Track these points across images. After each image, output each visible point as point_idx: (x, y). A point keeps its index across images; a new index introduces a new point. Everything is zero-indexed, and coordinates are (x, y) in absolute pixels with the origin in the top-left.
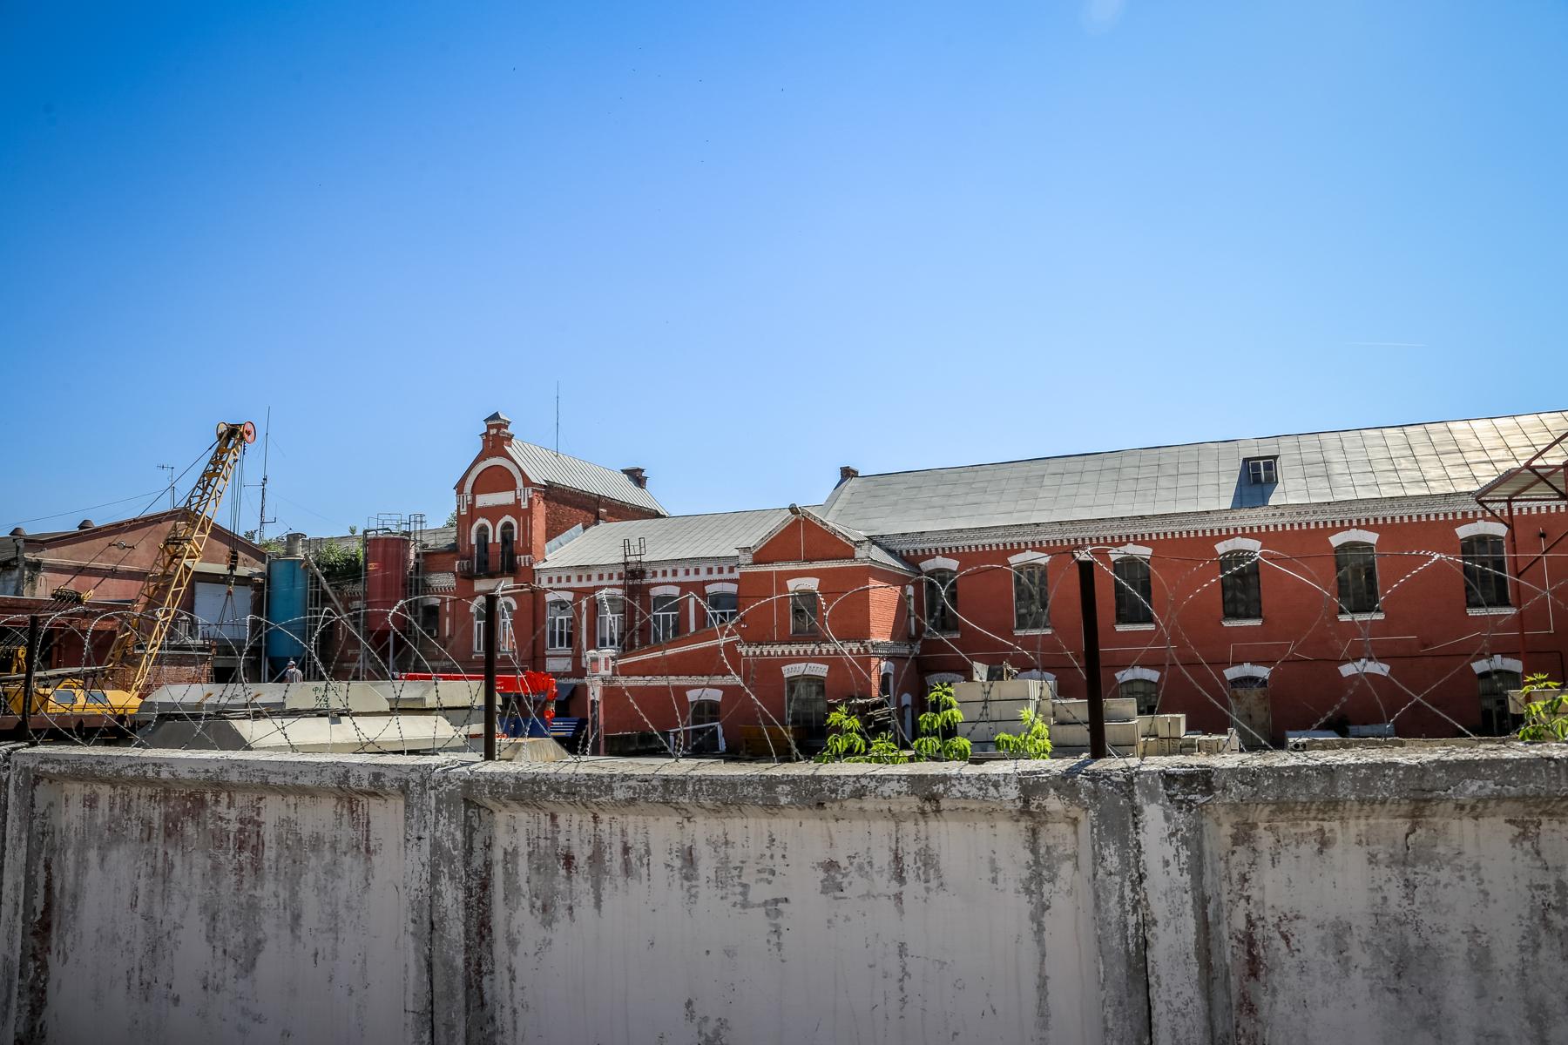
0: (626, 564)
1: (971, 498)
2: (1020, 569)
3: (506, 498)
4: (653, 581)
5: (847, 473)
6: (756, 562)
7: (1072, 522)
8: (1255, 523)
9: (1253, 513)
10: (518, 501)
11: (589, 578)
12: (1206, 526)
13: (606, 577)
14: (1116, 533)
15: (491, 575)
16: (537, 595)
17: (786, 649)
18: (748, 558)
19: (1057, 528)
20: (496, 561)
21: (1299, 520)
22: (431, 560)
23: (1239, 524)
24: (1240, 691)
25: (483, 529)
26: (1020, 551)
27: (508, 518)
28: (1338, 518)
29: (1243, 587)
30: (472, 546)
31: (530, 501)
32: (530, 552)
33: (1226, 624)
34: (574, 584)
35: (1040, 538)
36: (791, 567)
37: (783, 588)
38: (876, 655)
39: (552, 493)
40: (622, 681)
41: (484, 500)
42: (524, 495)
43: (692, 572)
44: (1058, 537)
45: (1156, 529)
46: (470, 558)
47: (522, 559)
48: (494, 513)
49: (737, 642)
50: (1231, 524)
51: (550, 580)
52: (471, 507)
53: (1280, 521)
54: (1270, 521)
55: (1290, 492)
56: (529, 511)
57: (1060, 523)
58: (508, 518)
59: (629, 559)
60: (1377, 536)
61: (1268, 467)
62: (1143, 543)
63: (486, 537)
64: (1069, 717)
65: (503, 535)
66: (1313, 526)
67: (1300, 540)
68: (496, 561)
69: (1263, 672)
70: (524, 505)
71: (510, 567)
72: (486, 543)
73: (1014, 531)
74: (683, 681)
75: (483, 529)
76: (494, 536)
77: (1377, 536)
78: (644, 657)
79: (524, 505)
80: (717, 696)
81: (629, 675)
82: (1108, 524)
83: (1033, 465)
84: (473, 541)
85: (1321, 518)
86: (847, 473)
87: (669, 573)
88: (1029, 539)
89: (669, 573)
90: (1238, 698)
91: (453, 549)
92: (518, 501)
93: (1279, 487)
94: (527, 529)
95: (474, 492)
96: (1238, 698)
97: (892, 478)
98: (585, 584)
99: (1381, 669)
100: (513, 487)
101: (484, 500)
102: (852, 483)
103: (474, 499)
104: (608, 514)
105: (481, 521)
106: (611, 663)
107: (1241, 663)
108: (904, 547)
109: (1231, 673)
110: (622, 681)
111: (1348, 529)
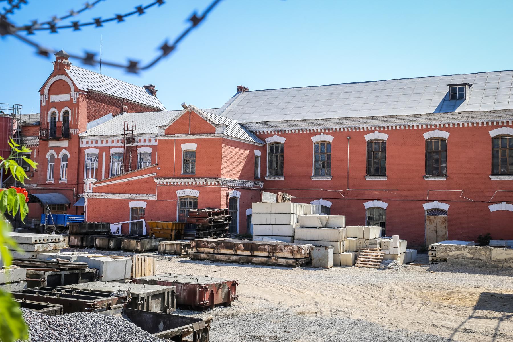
0: (125, 135)
1: (300, 104)
2: (317, 144)
3: (65, 97)
4: (139, 144)
5: (241, 89)
6: (166, 134)
7: (345, 118)
8: (446, 122)
9: (446, 116)
10: (71, 99)
11: (107, 142)
12: (356, 125)
13: (115, 141)
14: (369, 125)
15: (57, 139)
16: (80, 151)
17: (179, 181)
18: (162, 132)
19: (337, 121)
20: (60, 131)
21: (472, 121)
22: (25, 130)
23: (438, 122)
24: (432, 217)
25: (54, 114)
26: (318, 134)
27: (66, 108)
28: (495, 120)
29: (435, 156)
30: (48, 123)
31: (78, 99)
32: (77, 127)
33: (426, 179)
34: (99, 145)
35: (328, 127)
36: (183, 137)
37: (179, 148)
38: (224, 187)
39: (91, 95)
40: (97, 196)
41: (54, 98)
42: (74, 96)
43: (105, 142)
44: (338, 126)
45: (391, 123)
46: (47, 129)
47: (73, 131)
48: (59, 105)
49: (154, 177)
50: (433, 122)
51: (87, 142)
52: (48, 102)
53: (461, 121)
54: (455, 121)
55: (472, 105)
56: (77, 105)
57: (339, 119)
58: (66, 108)
59: (126, 132)
60: (387, 136)
61: (461, 90)
62: (384, 132)
63: (55, 118)
64: (308, 224)
65: (64, 118)
66: (480, 125)
67: (476, 131)
68: (60, 131)
69: (445, 207)
70: (75, 102)
71: (67, 135)
72: (55, 121)
73: (315, 122)
74: (127, 196)
75: (54, 114)
76: (60, 118)
77: (387, 136)
78: (109, 183)
79: (75, 102)
80: (144, 205)
81: (100, 193)
82: (365, 120)
83: (338, 87)
84: (49, 120)
85: (485, 120)
86: (241, 89)
87: (147, 140)
88: (322, 127)
89: (147, 140)
90: (430, 220)
91: (38, 124)
92: (71, 99)
93: (467, 101)
94: (76, 115)
95: (49, 93)
96: (430, 220)
97: (264, 92)
98: (105, 145)
99: (384, 205)
100: (69, 92)
101: (54, 98)
102: (244, 94)
103: (49, 98)
104: (129, 109)
105: (53, 110)
106: (92, 186)
107: (500, 202)
108: (258, 130)
109: (427, 206)
110: (97, 196)
111: (501, 127)
